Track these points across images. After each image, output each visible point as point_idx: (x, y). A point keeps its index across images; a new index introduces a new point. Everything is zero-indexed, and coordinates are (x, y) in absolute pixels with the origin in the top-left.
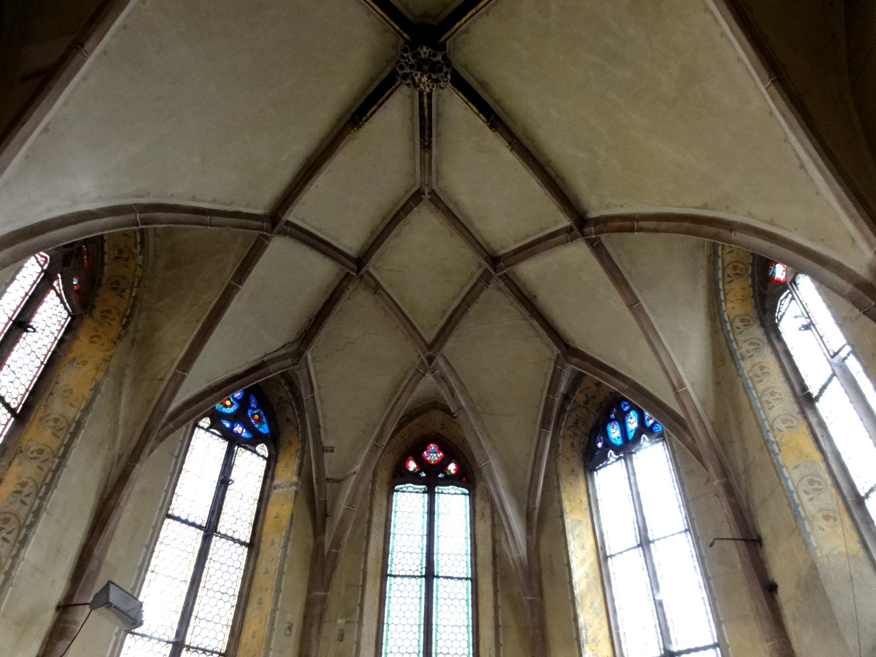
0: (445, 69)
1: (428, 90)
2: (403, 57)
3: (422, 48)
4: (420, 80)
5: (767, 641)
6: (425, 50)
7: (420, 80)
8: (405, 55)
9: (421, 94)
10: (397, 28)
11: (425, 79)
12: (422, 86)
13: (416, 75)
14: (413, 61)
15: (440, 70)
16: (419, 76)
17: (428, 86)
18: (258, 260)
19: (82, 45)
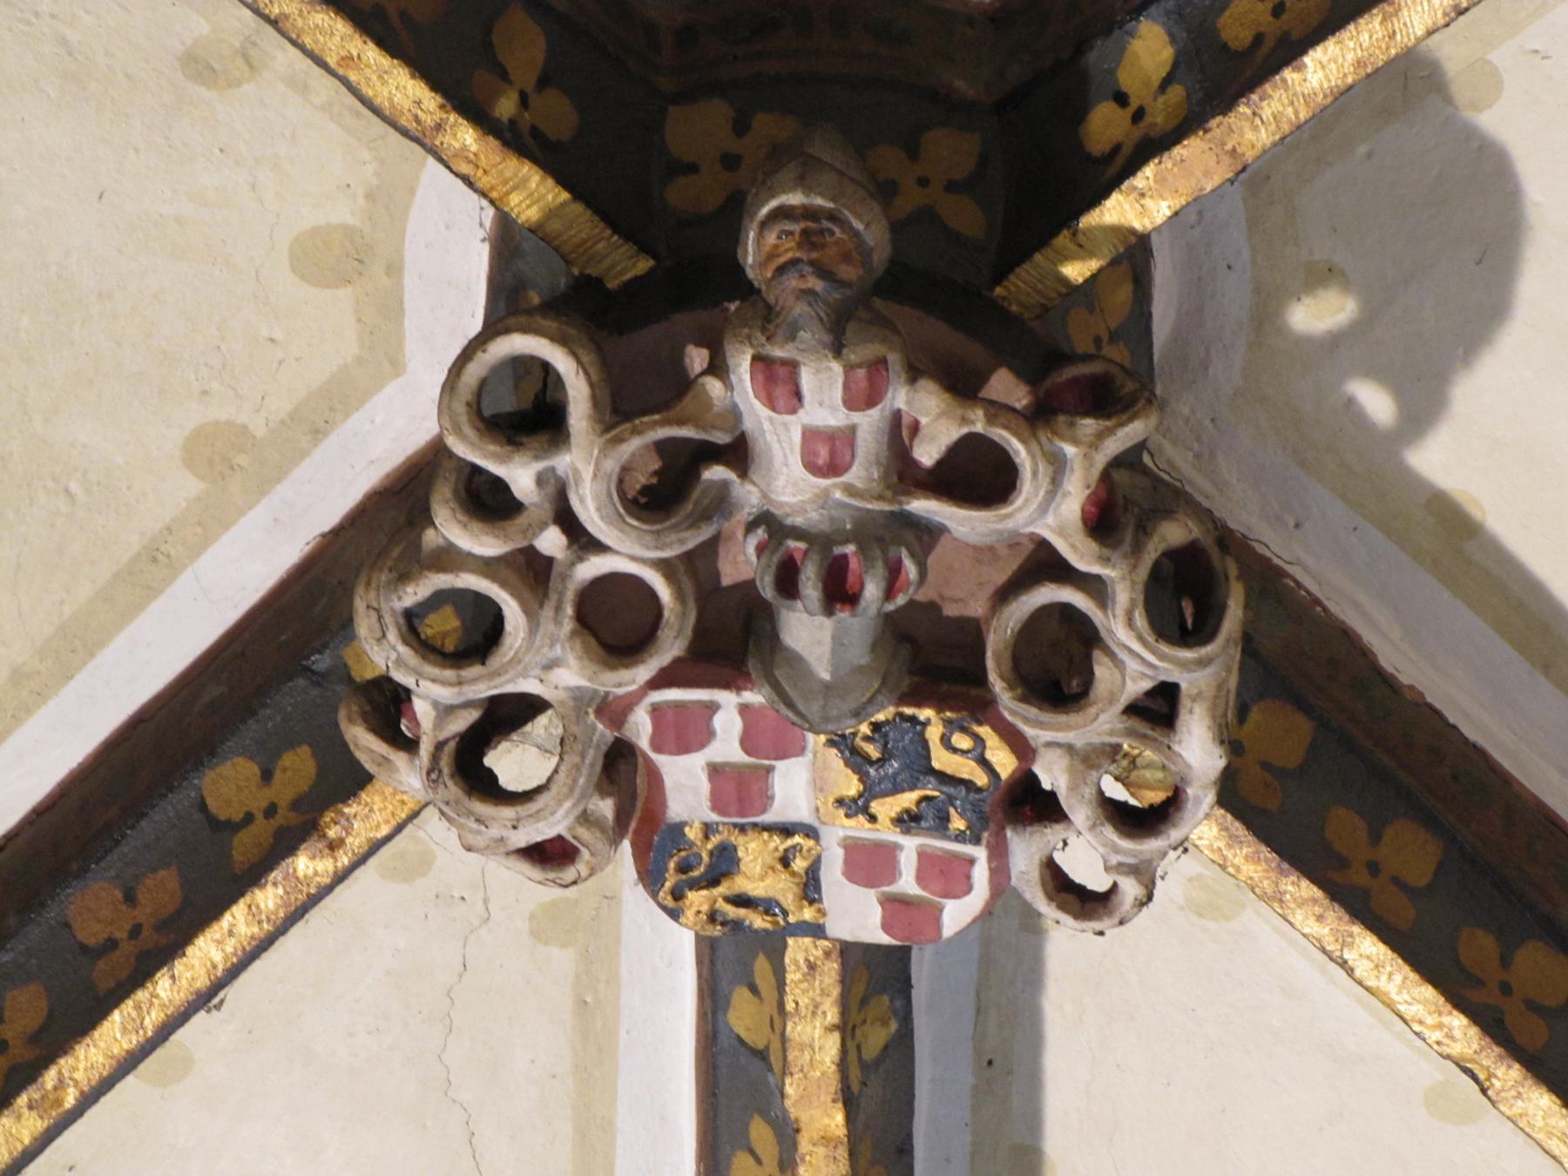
0: (1132, 659)
1: (856, 915)
2: (488, 501)
3: (780, 384)
4: (739, 790)
5: (911, 673)
6: (824, 391)
7: (739, 790)
8: (521, 476)
9: (736, 959)
10: (657, 417)
11: (802, 784)
12: (757, 868)
13: (685, 731)
14: (628, 552)
15: (1058, 666)
16: (727, 744)
17: (869, 864)
18: (1555, 813)
19: (43, 905)
